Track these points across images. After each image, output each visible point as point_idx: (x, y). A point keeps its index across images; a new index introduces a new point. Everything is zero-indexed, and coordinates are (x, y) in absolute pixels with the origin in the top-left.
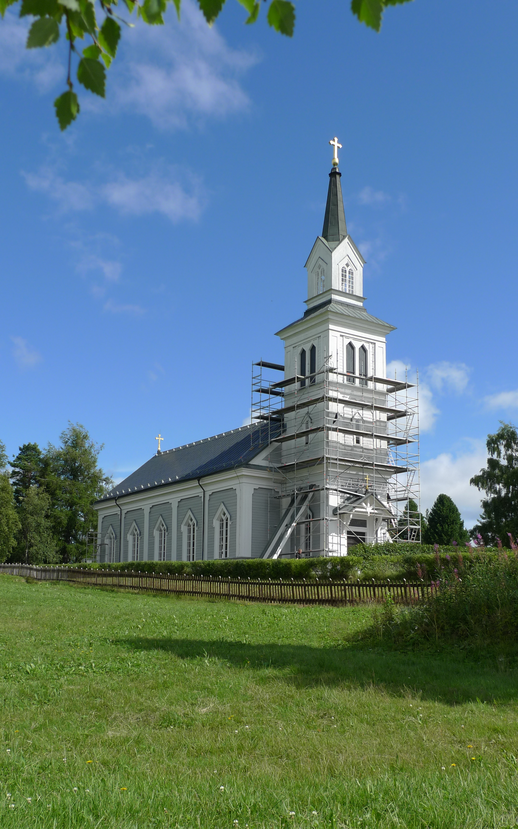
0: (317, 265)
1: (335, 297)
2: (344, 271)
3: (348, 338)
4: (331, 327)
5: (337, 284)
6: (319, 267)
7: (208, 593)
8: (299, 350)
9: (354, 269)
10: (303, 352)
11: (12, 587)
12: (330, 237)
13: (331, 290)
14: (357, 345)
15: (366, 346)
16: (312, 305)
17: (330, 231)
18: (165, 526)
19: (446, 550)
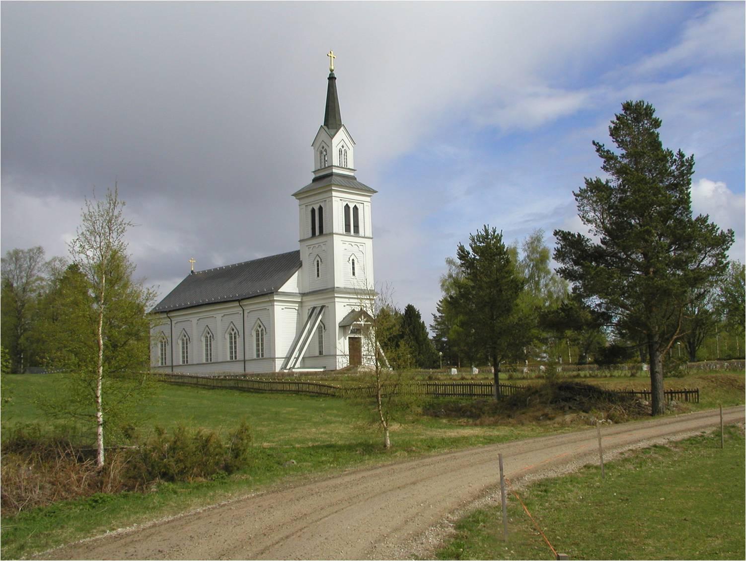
0: (321, 146)
1: (335, 170)
2: (340, 151)
3: (345, 201)
4: (334, 194)
5: (336, 162)
6: (323, 148)
7: (281, 391)
8: (310, 208)
9: (347, 149)
10: (313, 211)
11: (596, 383)
12: (330, 126)
13: (332, 166)
14: (352, 206)
15: (358, 205)
16: (318, 175)
17: (330, 122)
18: (187, 336)
19: (412, 465)
